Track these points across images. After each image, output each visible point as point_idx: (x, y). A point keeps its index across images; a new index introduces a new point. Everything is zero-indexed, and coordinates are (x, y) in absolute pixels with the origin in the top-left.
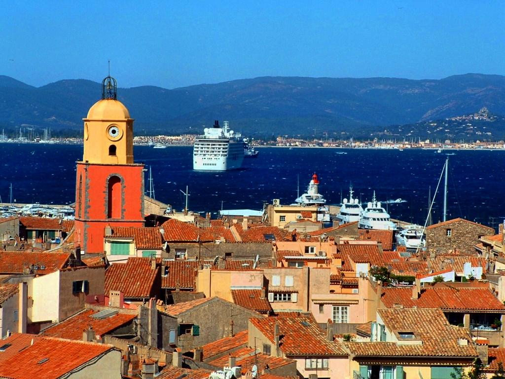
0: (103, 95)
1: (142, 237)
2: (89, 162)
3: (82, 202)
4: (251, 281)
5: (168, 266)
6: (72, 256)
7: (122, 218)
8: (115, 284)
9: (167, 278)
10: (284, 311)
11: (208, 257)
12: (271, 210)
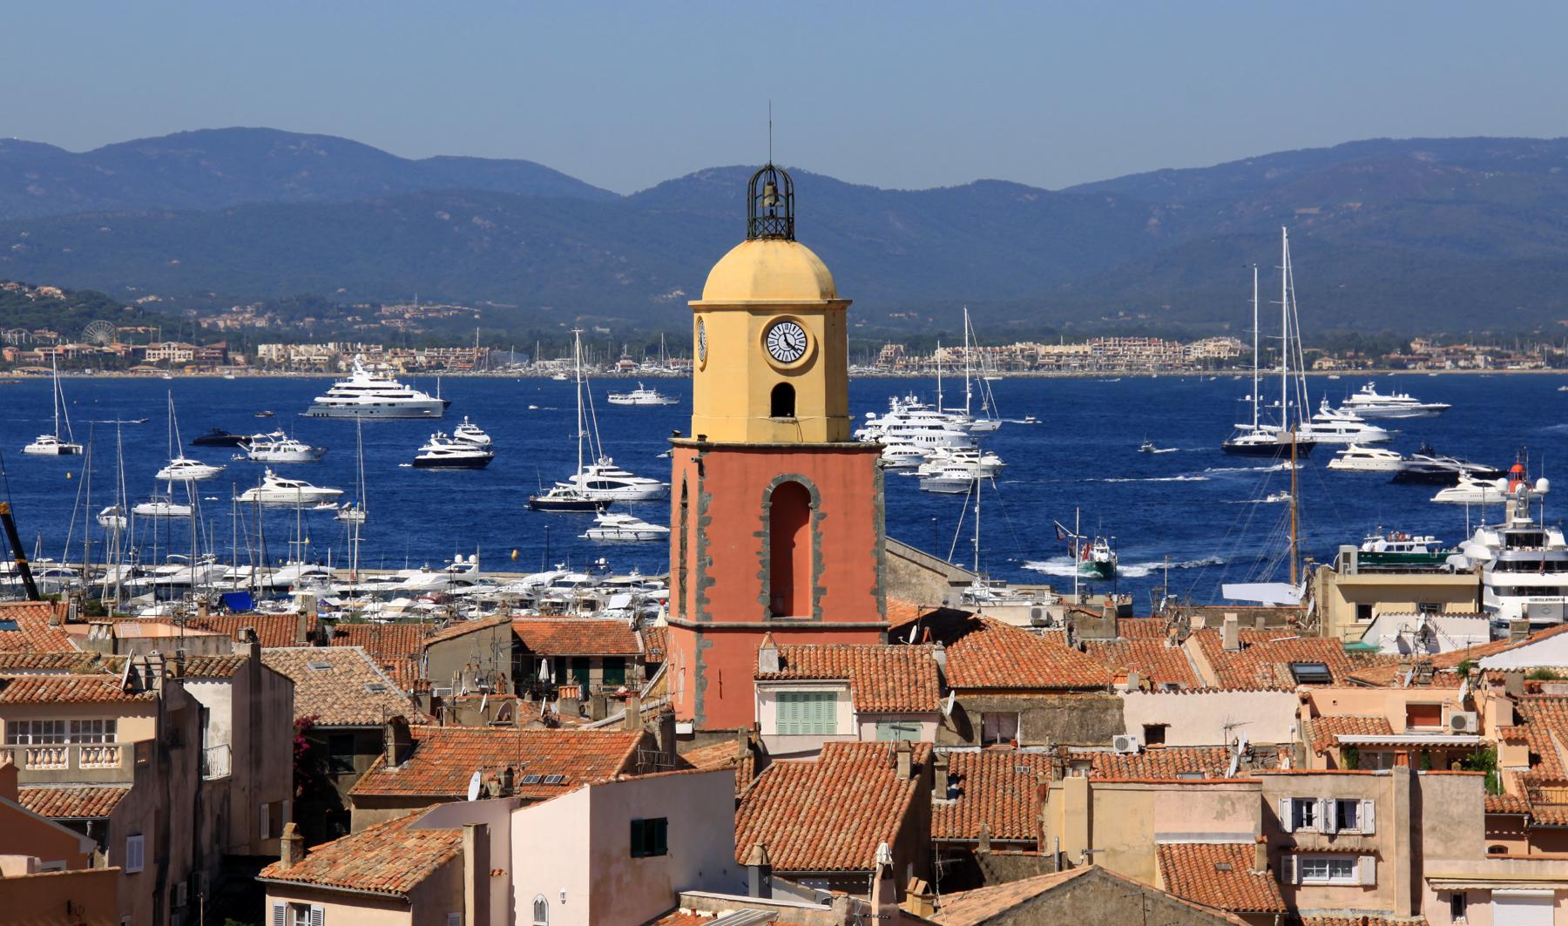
0: (753, 221)
1: (874, 677)
2: (707, 440)
3: (688, 566)
4: (1220, 816)
5: (960, 773)
6: (648, 739)
7: (816, 616)
8: (781, 828)
9: (954, 809)
10: (1333, 915)
11: (1088, 740)
12: (1325, 585)
